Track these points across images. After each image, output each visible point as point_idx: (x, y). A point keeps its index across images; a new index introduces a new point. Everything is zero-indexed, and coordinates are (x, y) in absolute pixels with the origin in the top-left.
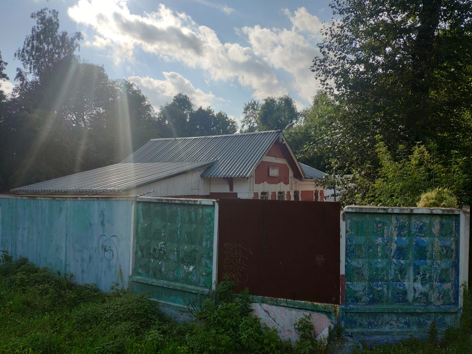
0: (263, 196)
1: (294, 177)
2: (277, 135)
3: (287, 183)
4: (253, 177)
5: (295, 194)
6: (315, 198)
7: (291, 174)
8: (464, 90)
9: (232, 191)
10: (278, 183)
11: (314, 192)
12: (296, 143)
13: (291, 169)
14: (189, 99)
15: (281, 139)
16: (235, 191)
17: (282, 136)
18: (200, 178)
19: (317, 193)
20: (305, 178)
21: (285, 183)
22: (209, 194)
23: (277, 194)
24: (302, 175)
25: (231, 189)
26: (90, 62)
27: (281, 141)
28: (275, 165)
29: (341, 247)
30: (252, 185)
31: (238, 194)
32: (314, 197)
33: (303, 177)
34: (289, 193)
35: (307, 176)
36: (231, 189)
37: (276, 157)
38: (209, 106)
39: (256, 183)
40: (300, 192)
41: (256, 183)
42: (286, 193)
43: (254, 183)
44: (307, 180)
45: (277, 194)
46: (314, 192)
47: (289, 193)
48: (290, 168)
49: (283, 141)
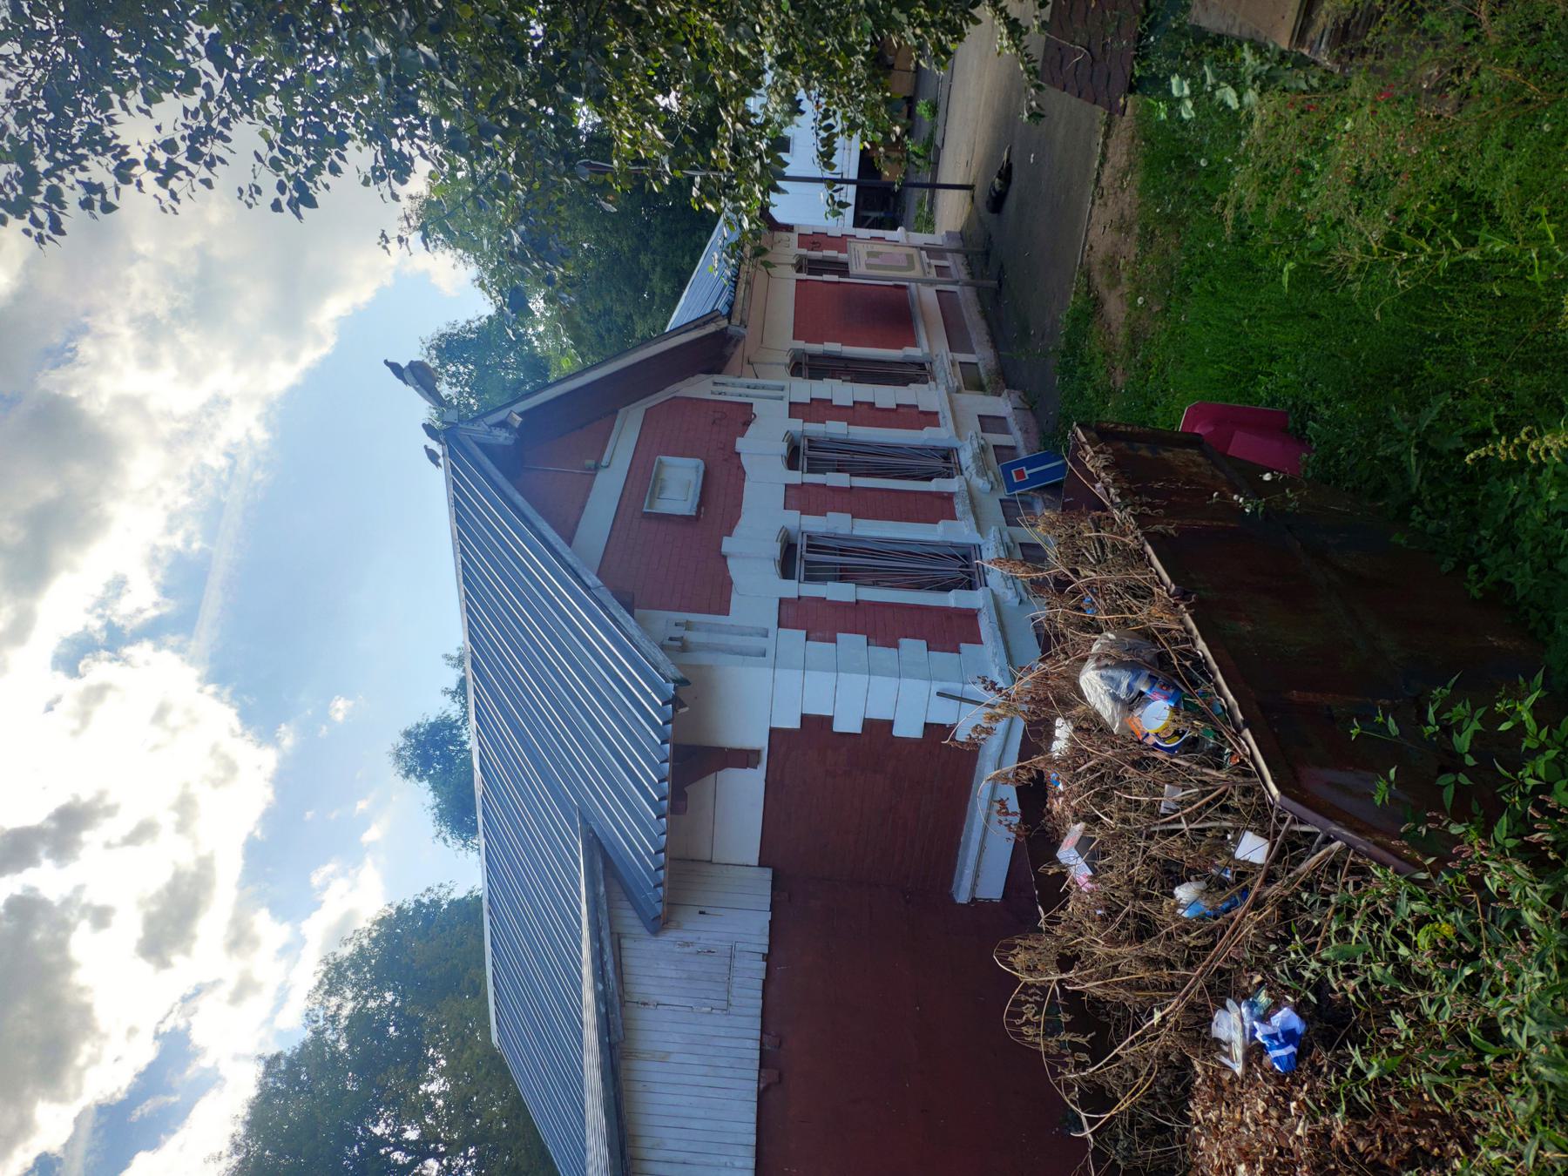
0: (803, 462)
1: (719, 372)
2: (468, 454)
3: (742, 416)
4: (688, 626)
5: (805, 372)
6: (833, 272)
7: (701, 387)
8: (755, 158)
9: (757, 753)
10: (740, 467)
11: (803, 276)
12: (609, 331)
13: (678, 386)
14: (418, 726)
15: (497, 432)
16: (760, 741)
17: (481, 428)
18: (671, 936)
19: (811, 261)
20: (729, 316)
21: (747, 424)
22: (767, 874)
23: (796, 477)
24: (711, 328)
25: (745, 758)
26: (243, 1112)
27: (502, 436)
28: (642, 478)
29: (543, 401)
30: (735, 641)
31: (777, 725)
32: (826, 277)
33: (724, 323)
34: (795, 409)
35: (721, 305)
36: (745, 758)
37: (597, 468)
38: (445, 661)
39: (725, 611)
40: (801, 345)
41: (725, 611)
42: (797, 425)
43: (721, 619)
44: (738, 307)
45: (796, 477)
46: (803, 276)
47: (795, 409)
48: (670, 389)
49: (503, 424)
